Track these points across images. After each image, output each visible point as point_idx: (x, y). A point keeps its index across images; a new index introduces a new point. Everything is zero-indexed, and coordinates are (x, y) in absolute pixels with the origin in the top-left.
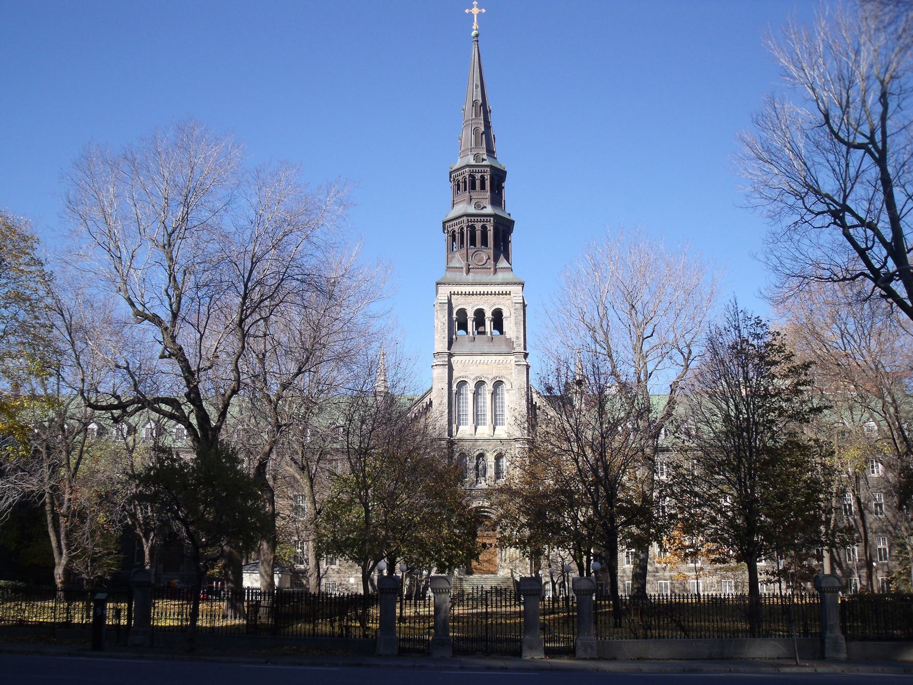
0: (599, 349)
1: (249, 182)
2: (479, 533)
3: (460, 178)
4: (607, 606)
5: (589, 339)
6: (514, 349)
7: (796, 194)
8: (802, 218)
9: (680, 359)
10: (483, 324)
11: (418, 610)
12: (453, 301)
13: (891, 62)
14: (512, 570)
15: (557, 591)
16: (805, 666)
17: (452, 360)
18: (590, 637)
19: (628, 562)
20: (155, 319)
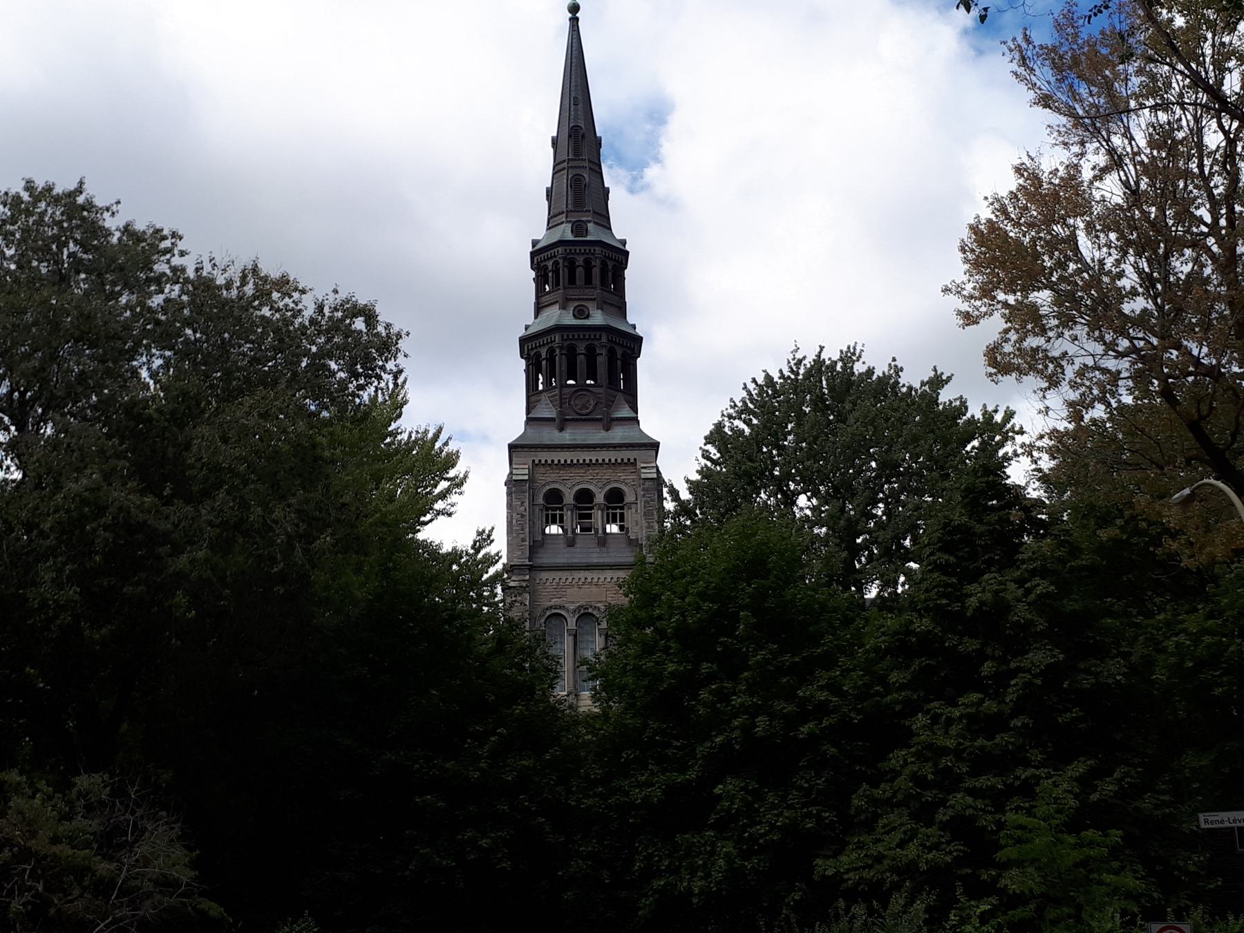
13: (29, 503)
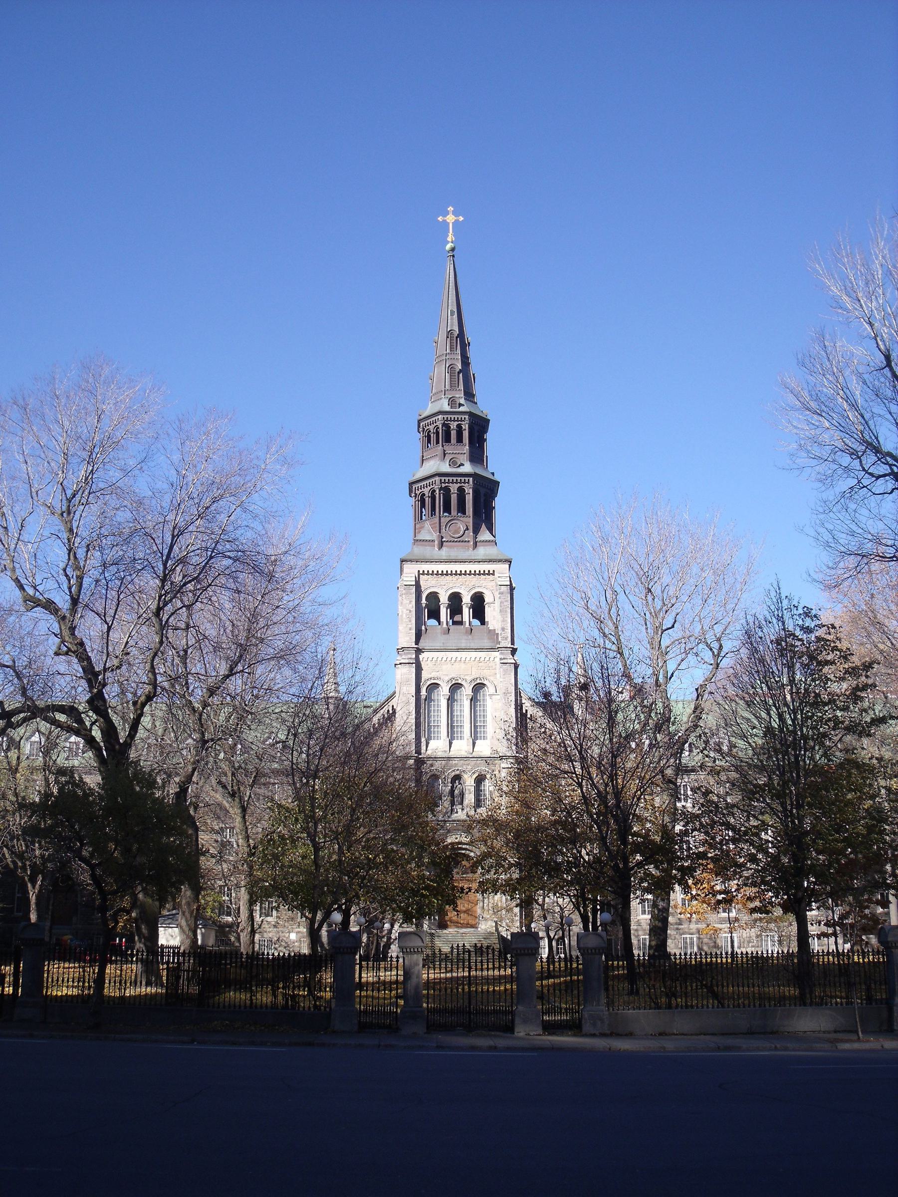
0: (609, 645)
2: (456, 876)
3: (431, 427)
4: (619, 967)
5: (596, 633)
6: (499, 643)
7: (853, 454)
8: (859, 482)
9: (708, 656)
10: (460, 612)
14: (496, 922)
15: (555, 949)
16: (868, 1041)
17: (421, 657)
18: (600, 1007)
19: (644, 912)
20: (49, 606)
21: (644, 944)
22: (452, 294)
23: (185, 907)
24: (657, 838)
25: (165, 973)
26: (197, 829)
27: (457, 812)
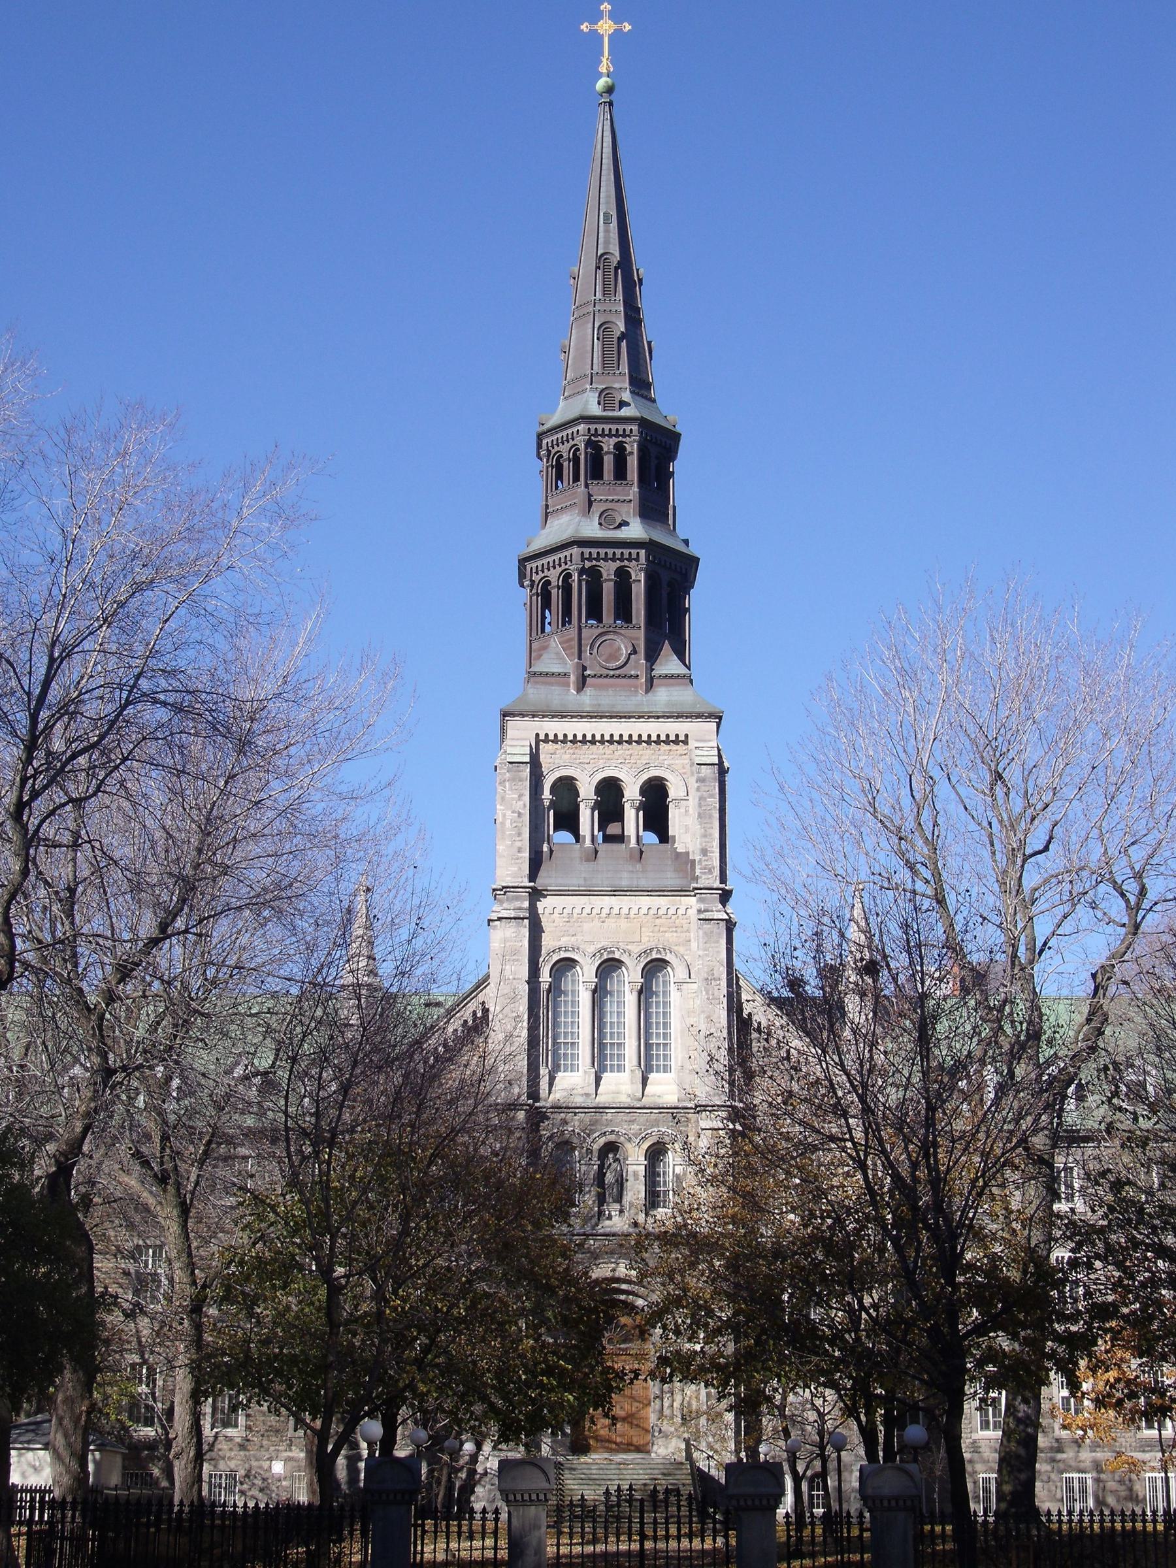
0: (920, 886)
1: (44, 457)
2: (609, 1348)
3: (564, 449)
5: (897, 863)
6: (696, 879)
9: (1116, 908)
10: (619, 816)
11: (454, 1545)
12: (543, 758)
14: (687, 1442)
15: (805, 1497)
17: (540, 906)
21: (987, 1490)
22: (608, 180)
23: (62, 1409)
24: (1014, 1275)
25: (23, 1541)
26: (91, 1249)
27: (610, 1218)
